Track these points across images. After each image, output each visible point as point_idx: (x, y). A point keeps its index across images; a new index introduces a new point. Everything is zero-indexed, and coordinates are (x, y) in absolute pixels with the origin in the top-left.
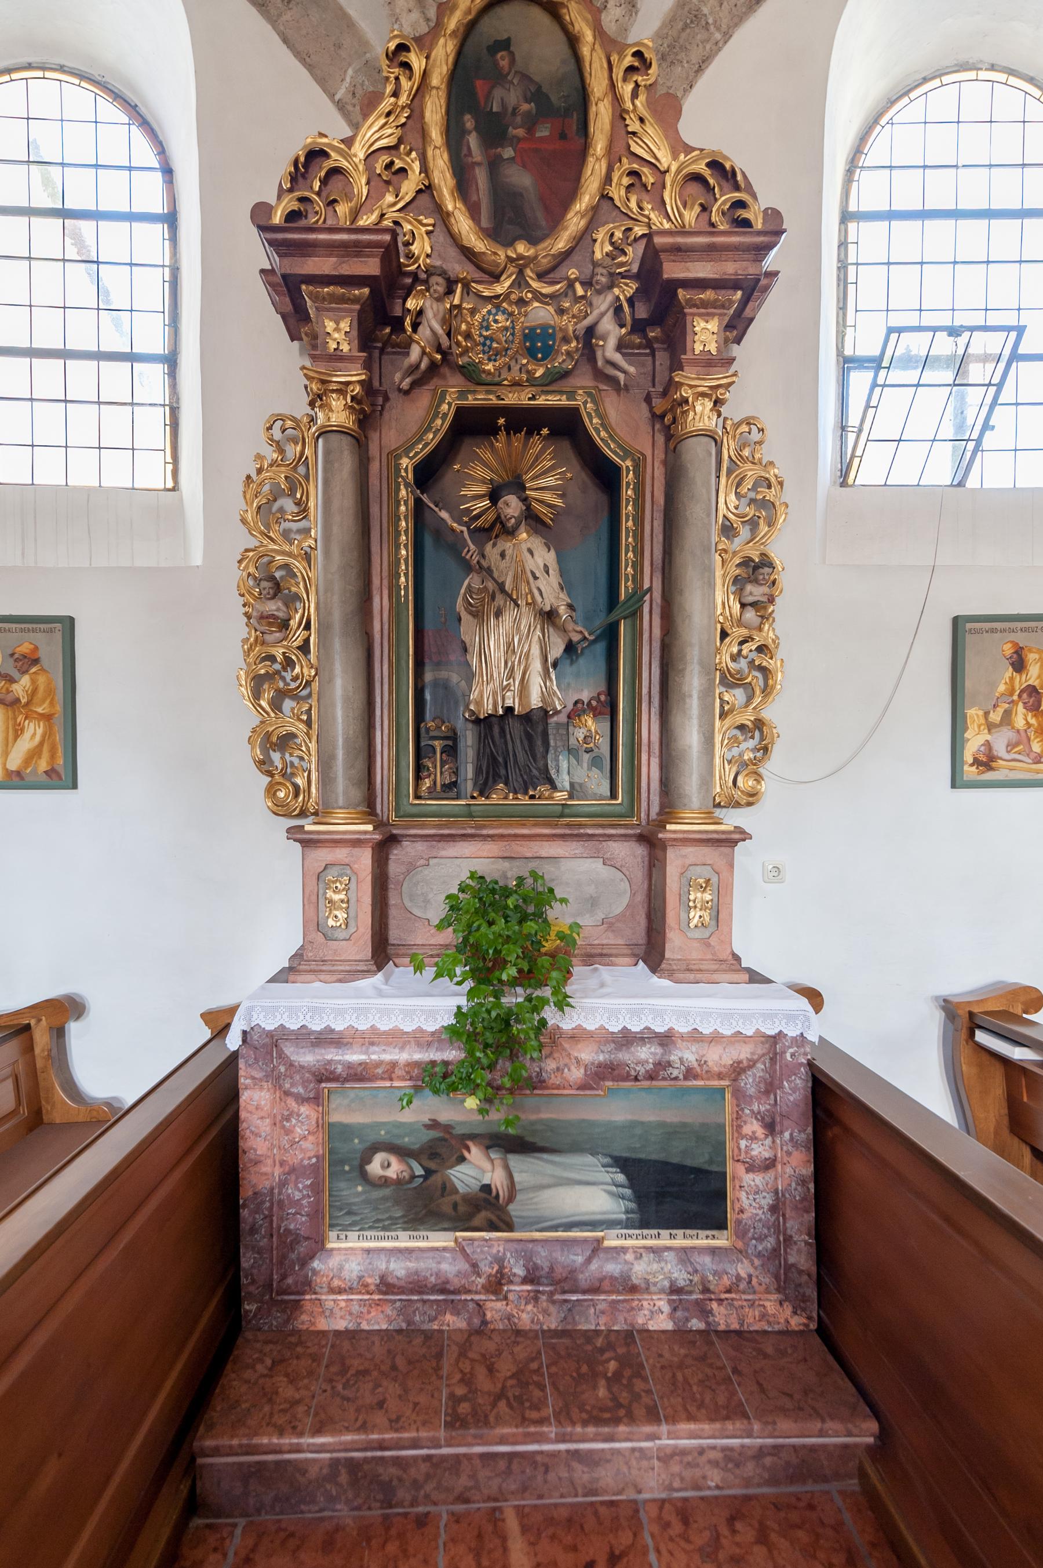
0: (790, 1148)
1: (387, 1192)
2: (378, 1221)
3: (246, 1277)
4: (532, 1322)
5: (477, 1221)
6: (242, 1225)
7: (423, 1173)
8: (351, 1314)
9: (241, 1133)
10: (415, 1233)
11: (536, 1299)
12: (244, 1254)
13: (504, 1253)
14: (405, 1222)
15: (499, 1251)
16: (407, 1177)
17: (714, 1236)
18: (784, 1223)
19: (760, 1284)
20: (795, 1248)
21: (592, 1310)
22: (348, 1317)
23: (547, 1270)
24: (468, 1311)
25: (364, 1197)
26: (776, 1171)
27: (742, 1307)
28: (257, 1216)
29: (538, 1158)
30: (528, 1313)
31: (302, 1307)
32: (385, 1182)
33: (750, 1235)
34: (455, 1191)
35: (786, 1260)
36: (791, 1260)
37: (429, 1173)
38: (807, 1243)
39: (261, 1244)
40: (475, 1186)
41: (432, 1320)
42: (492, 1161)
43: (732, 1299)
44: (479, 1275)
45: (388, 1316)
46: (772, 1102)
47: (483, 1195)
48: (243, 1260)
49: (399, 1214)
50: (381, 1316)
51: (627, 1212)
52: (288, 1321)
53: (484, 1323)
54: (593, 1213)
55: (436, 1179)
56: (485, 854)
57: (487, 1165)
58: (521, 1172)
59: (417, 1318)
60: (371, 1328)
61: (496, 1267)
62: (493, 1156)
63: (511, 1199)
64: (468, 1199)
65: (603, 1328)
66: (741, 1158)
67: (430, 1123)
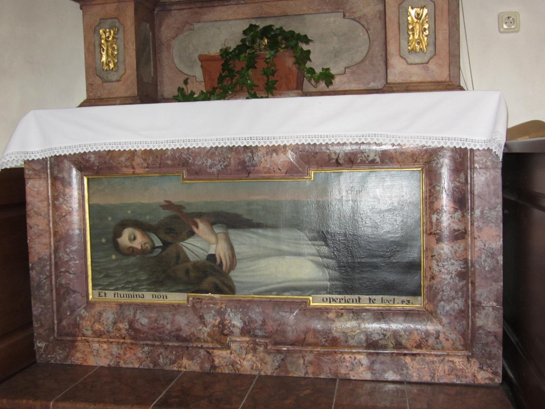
0: (481, 224)
1: (132, 260)
2: (128, 283)
3: (37, 322)
4: (252, 368)
5: (205, 285)
6: (32, 283)
7: (161, 244)
8: (112, 355)
9: (28, 213)
10: (157, 294)
11: (255, 350)
12: (34, 304)
13: (226, 309)
14: (149, 284)
15: (221, 308)
16: (149, 248)
17: (409, 301)
18: (474, 290)
19: (447, 340)
20: (483, 312)
21: (302, 361)
22: (110, 357)
23: (260, 323)
24: (200, 357)
25: (116, 264)
26: (467, 243)
27: (433, 362)
28: (41, 276)
29: (254, 233)
30: (248, 361)
31: (76, 347)
32: (132, 252)
33: (439, 297)
34: (187, 259)
35: (473, 323)
36: (479, 323)
37: (166, 244)
38: (494, 308)
39: (46, 297)
40: (203, 256)
41: (173, 362)
42: (216, 235)
43: (424, 355)
44: (205, 325)
45: (139, 358)
46: (463, 180)
47: (209, 263)
48: (34, 309)
49: (144, 278)
50: (134, 357)
51: (331, 280)
52: (67, 357)
53: (214, 367)
54: (301, 280)
55: (171, 250)
56: (240, 16)
57: (213, 239)
58: (242, 244)
59: (161, 360)
60: (127, 366)
61: (219, 319)
62: (217, 230)
63: (232, 266)
64: (197, 266)
65: (311, 376)
66: (433, 231)
67: (165, 204)
